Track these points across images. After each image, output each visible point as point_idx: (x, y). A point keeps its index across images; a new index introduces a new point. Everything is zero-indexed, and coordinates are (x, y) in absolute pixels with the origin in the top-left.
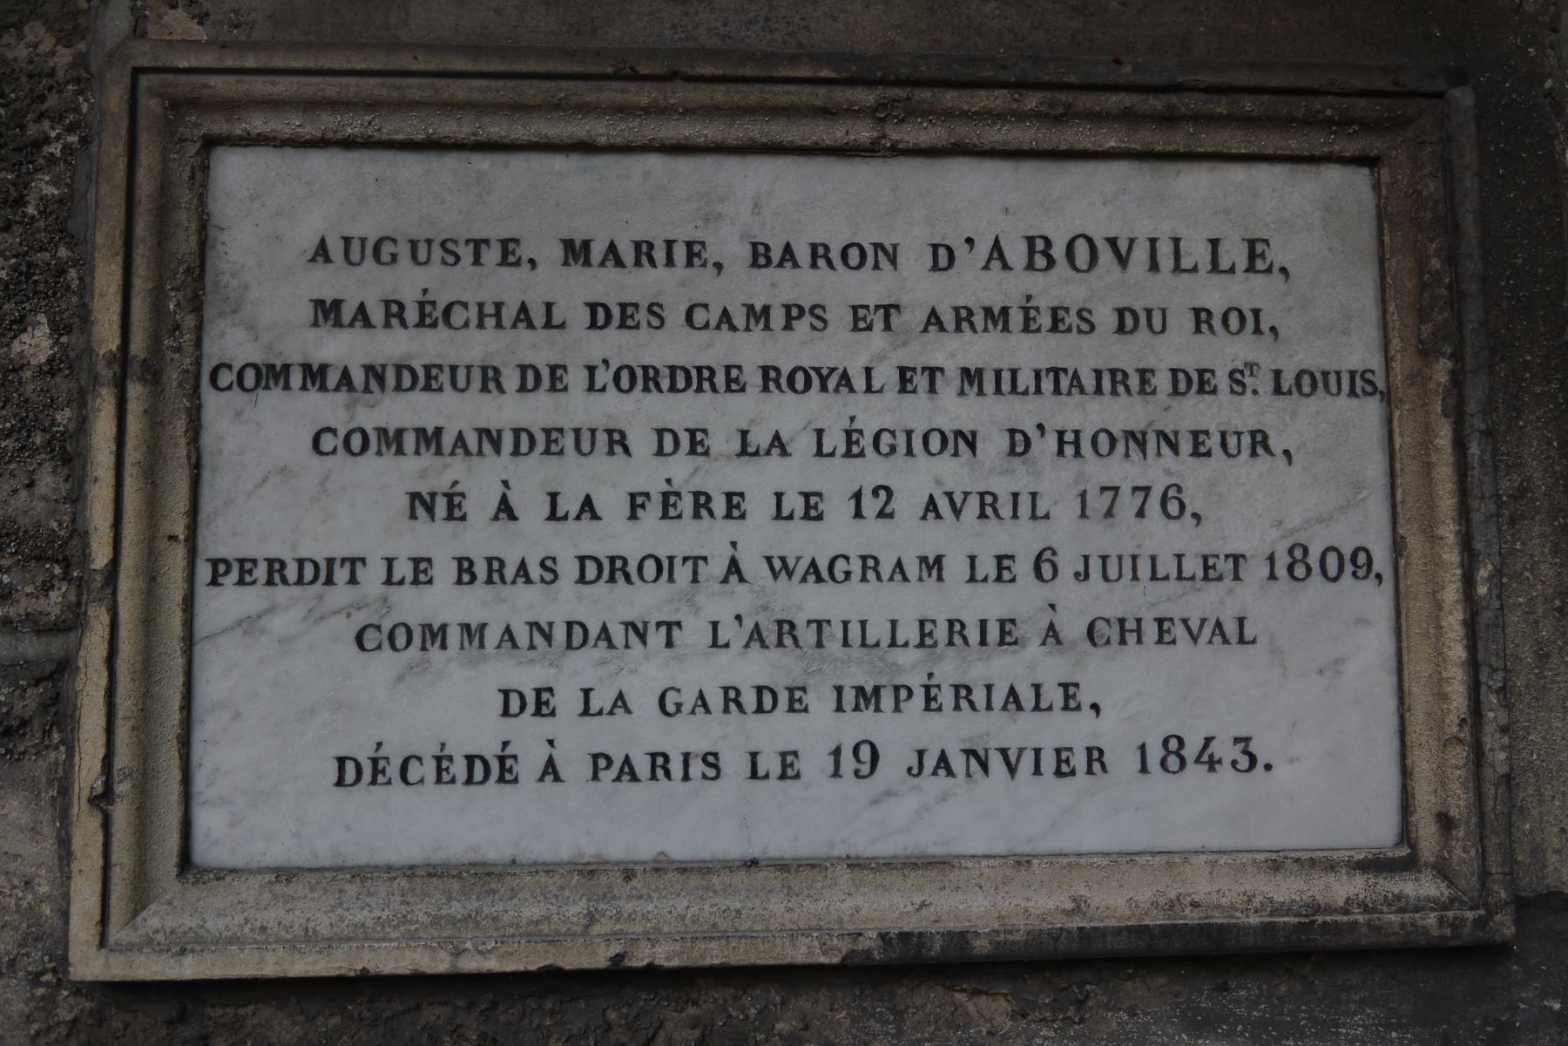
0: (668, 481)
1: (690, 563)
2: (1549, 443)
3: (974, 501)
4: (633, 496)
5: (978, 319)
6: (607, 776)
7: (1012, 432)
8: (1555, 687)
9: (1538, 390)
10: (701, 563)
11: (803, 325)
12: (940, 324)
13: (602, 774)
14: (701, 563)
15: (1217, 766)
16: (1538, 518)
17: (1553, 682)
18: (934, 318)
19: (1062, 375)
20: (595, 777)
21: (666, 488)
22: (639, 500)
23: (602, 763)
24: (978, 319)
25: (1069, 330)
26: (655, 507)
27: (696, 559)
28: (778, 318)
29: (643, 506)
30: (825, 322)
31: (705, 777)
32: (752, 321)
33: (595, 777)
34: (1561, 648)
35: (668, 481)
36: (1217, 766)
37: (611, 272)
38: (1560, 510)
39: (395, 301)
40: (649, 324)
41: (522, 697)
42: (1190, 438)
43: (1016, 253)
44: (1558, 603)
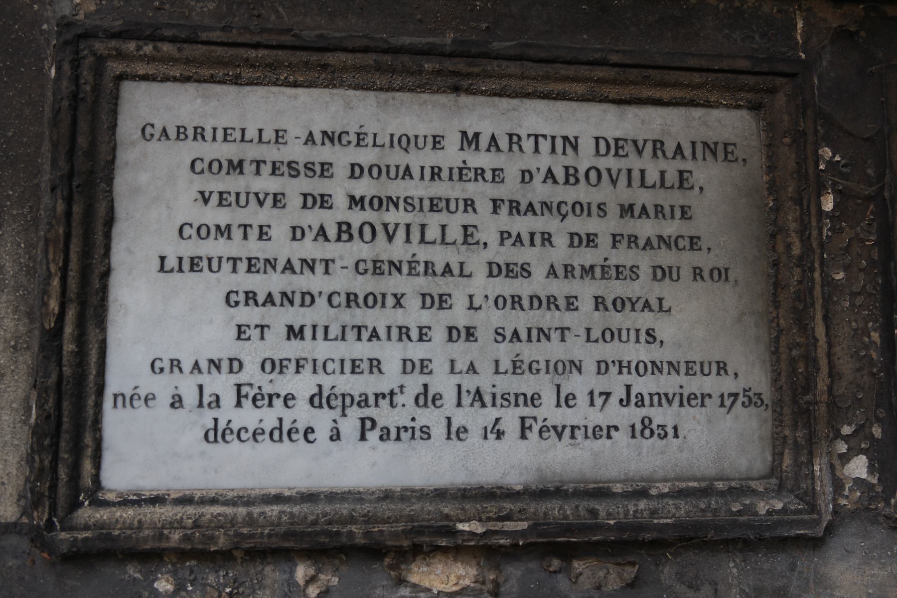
0: (464, 162)
2: (19, 245)
3: (649, 146)
6: (373, 436)
7: (424, 295)
8: (6, 395)
9: (15, 212)
13: (369, 435)
16: (6, 290)
17: (5, 391)
19: (363, 330)
20: (363, 438)
21: (462, 165)
23: (368, 424)
29: (303, 366)
31: (422, 438)
33: (363, 438)
34: (13, 371)
35: (464, 162)
37: (288, 275)
38: (22, 286)
41: (432, 297)
43: (332, 232)
44: (12, 343)
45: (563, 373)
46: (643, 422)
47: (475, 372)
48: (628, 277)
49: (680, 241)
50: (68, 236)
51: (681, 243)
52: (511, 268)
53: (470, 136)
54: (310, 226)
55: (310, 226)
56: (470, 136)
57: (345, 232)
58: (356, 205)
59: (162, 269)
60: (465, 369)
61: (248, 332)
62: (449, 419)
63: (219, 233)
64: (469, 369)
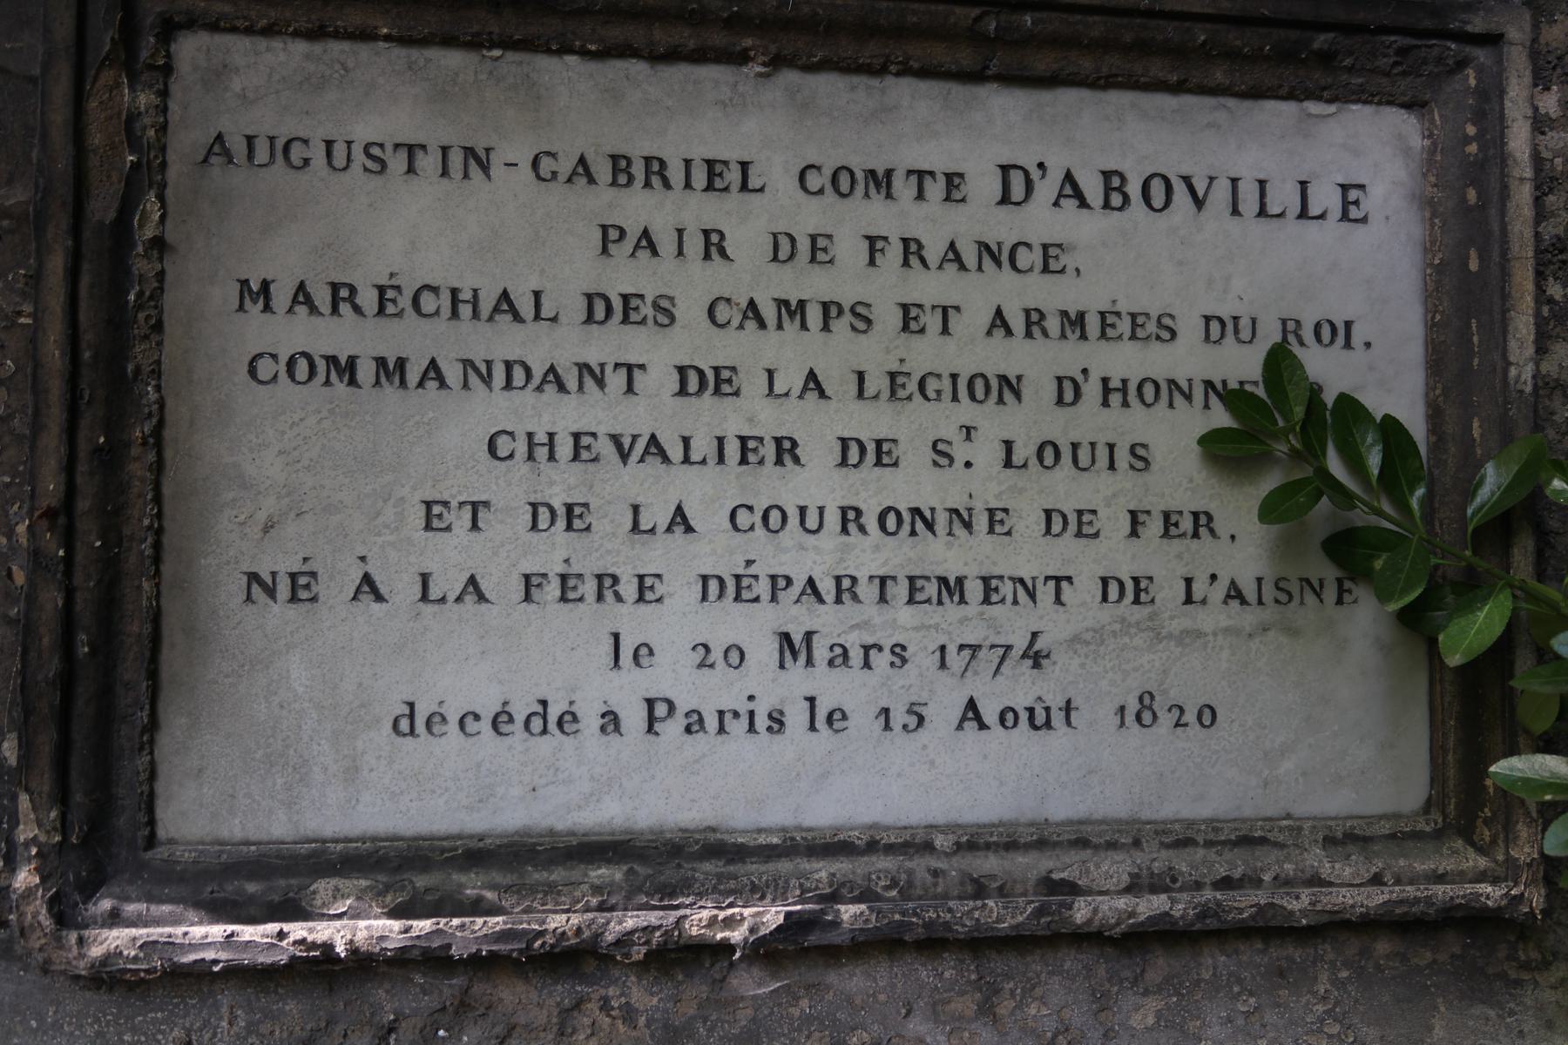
1: (1052, 583)
4: (527, 577)
5: (1053, 324)
10: (1064, 584)
11: (841, 326)
12: (309, 302)
14: (1064, 584)
15: (1044, 662)
18: (999, 320)
22: (535, 581)
24: (1053, 324)
25: (643, 322)
26: (553, 589)
27: (1058, 579)
28: (814, 315)
30: (869, 321)
32: (247, 301)
36: (1044, 662)
39: (345, 284)
40: (656, 322)
42: (571, 440)
45: (310, 379)
46: (1141, 699)
47: (689, 529)
48: (650, 321)
49: (1022, 253)
50: (37, 427)
51: (1024, 258)
52: (913, 315)
53: (255, 287)
54: (1041, 165)
55: (1041, 165)
56: (255, 287)
57: (344, 299)
58: (255, 302)
59: (1008, 463)
60: (663, 521)
61: (449, 517)
62: (616, 636)
63: (872, 185)
64: (672, 523)
